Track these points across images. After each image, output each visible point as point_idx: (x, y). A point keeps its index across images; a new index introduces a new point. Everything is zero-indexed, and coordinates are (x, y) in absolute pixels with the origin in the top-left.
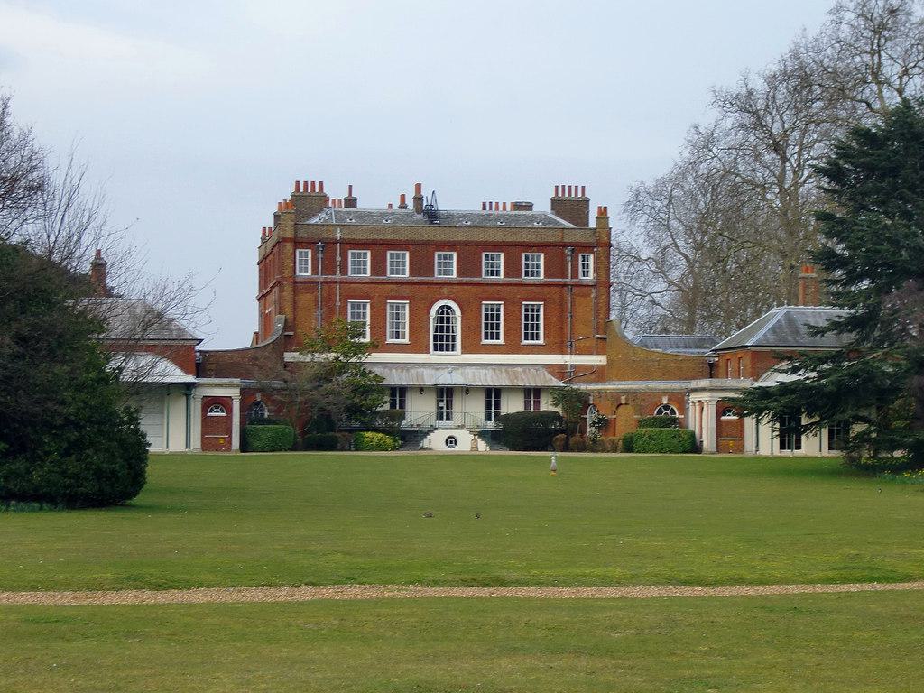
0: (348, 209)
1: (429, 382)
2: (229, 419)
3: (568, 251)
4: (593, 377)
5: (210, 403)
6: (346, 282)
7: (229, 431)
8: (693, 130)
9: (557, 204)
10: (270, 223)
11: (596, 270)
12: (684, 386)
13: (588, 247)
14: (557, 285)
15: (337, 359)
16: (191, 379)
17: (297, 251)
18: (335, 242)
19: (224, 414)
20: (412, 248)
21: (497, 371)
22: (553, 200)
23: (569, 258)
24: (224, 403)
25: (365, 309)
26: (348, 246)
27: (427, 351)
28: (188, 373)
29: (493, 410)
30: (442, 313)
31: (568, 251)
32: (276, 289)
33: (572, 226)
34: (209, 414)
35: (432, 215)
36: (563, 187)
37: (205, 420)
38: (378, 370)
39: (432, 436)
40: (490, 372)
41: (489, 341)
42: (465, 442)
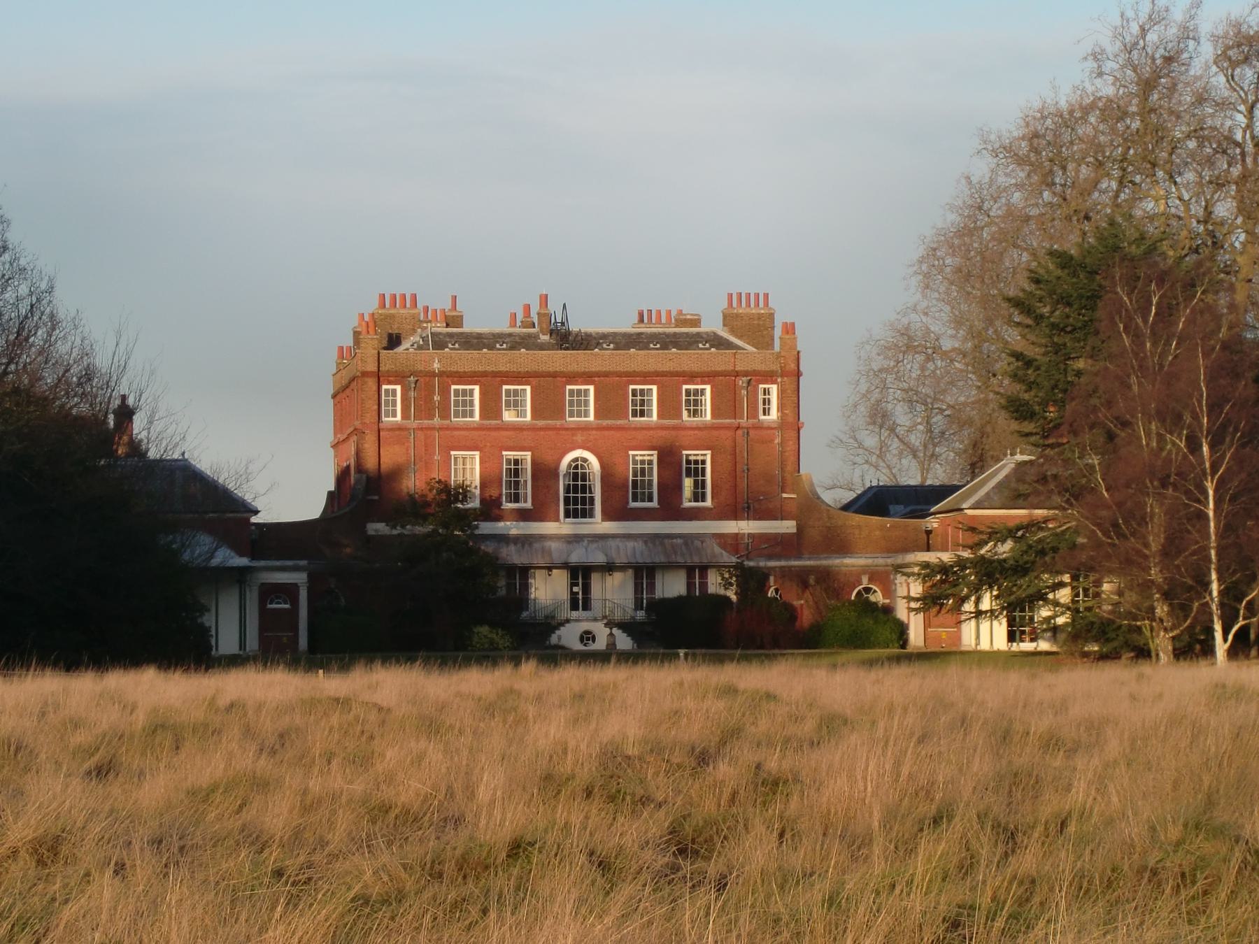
2: (295, 610)
3: (742, 381)
4: (778, 549)
5: (270, 592)
6: (447, 429)
7: (295, 629)
8: (963, 181)
10: (349, 341)
11: (781, 407)
12: (889, 561)
13: (769, 377)
14: (727, 428)
15: (434, 530)
16: (243, 561)
18: (432, 374)
19: (287, 606)
20: (534, 381)
22: (725, 316)
23: (744, 392)
24: (289, 591)
26: (449, 380)
28: (241, 555)
31: (742, 381)
32: (355, 438)
34: (269, 606)
36: (757, 296)
37: (263, 613)
38: (488, 547)
39: (563, 631)
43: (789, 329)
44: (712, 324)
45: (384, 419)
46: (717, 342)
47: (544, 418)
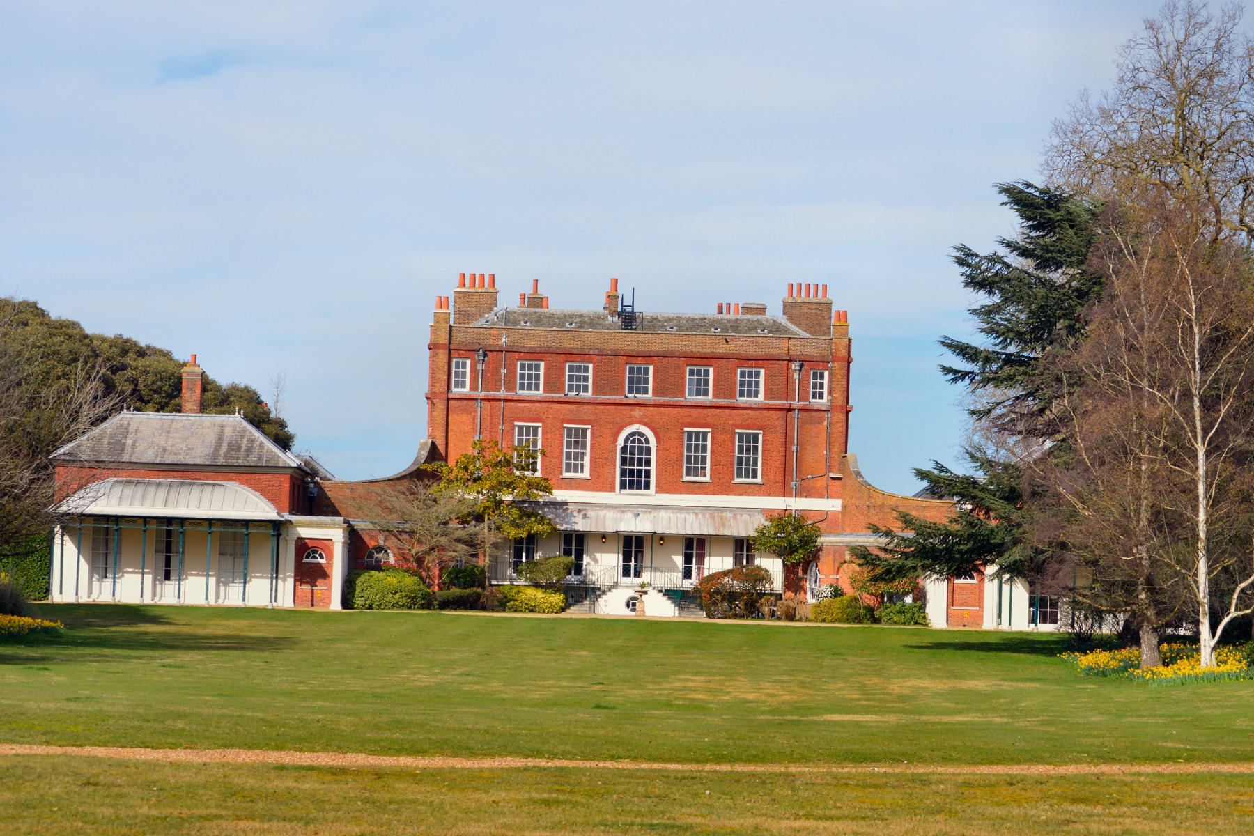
0: (532, 310)
1: (610, 528)
9: (789, 308)
11: (830, 393)
17: (454, 361)
21: (700, 516)
23: (796, 376)
25: (535, 434)
27: (612, 489)
29: (632, 564)
30: (633, 441)
31: (795, 366)
33: (808, 336)
34: (305, 560)
35: (629, 319)
40: (690, 517)
41: (691, 478)
42: (659, 608)
43: (843, 316)
44: (775, 312)
45: (454, 390)
46: (776, 328)
47: (605, 394)
